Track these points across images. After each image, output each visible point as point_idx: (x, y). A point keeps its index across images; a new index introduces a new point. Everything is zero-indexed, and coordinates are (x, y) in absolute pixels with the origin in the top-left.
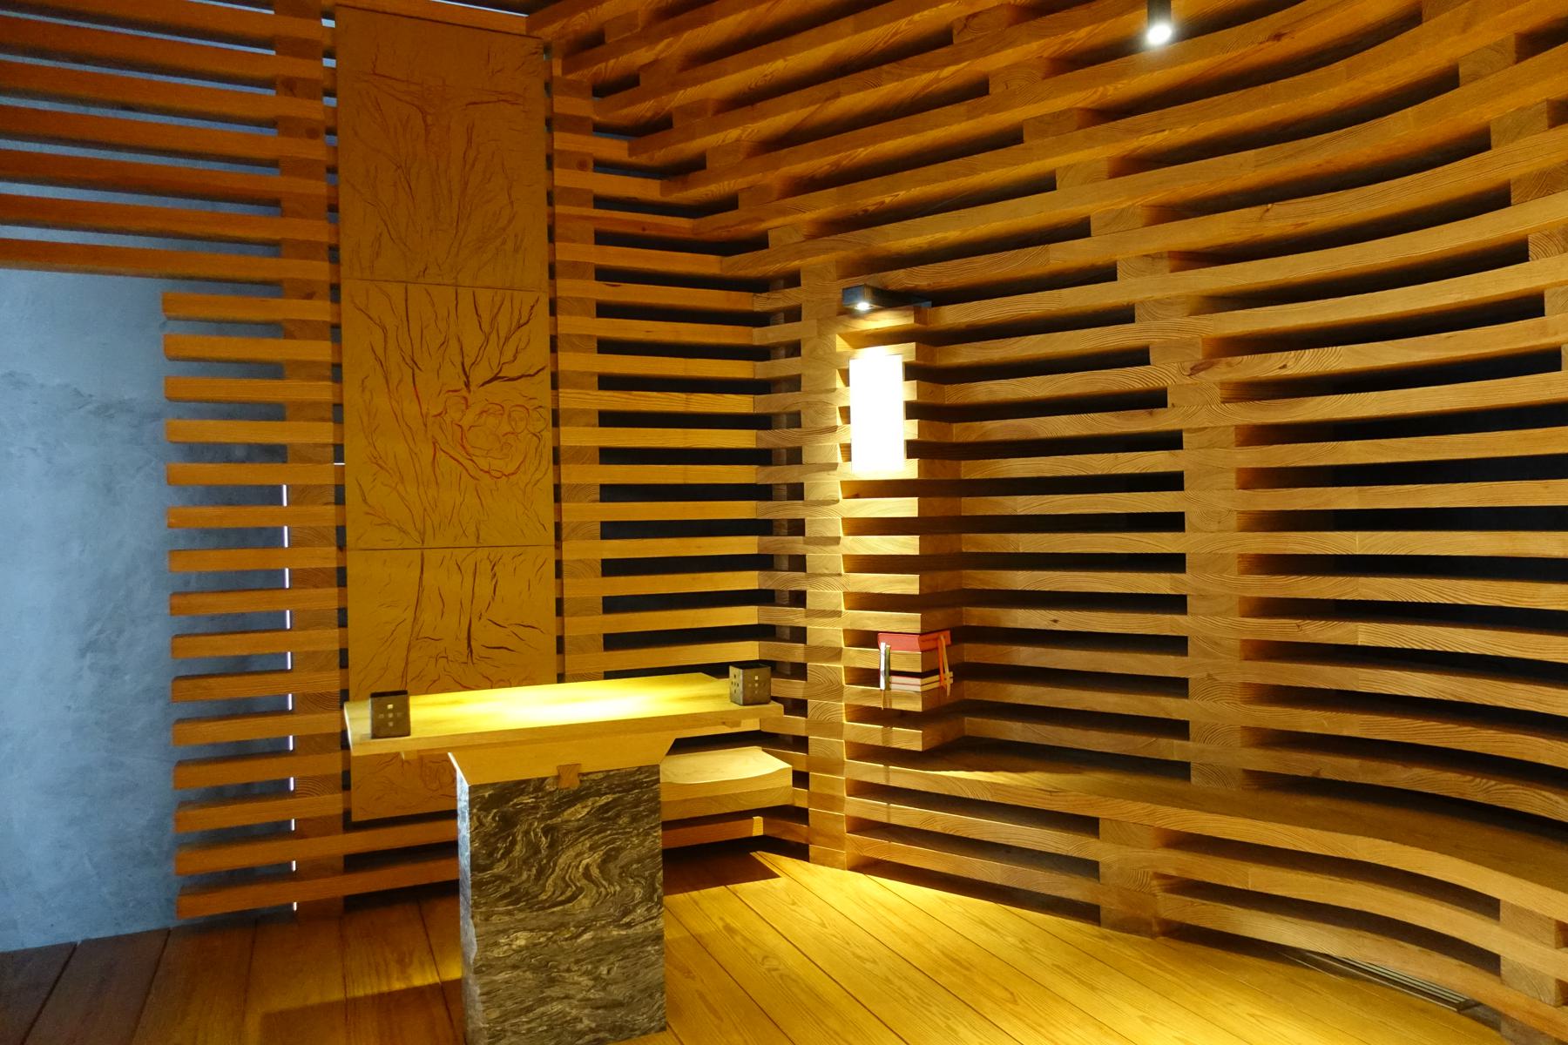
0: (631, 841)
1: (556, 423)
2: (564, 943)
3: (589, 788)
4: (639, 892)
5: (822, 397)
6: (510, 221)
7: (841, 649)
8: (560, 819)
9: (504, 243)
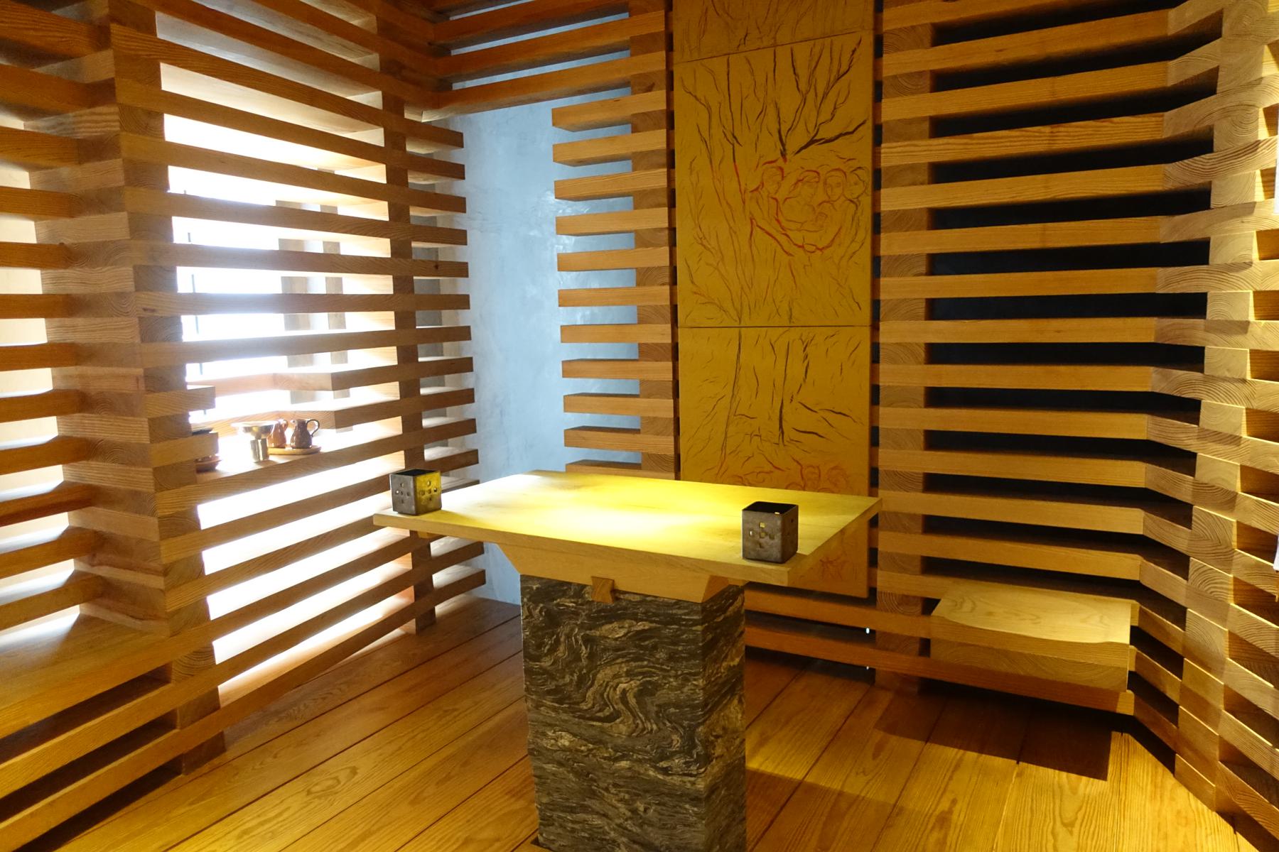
0: (669, 682)
2: (602, 760)
3: (625, 608)
4: (677, 741)
7: (1235, 495)
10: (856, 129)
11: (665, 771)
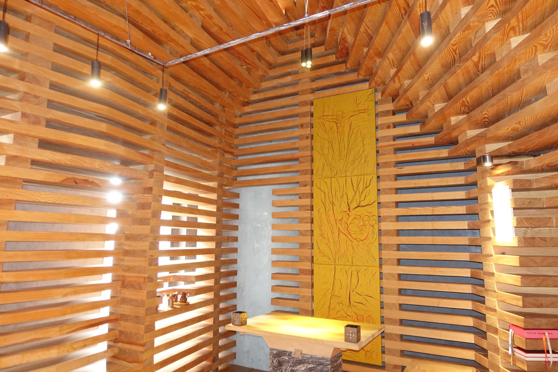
1: (379, 221)
3: (305, 360)
5: (485, 206)
6: (363, 152)
7: (497, 329)
8: (296, 368)
9: (361, 160)
10: (372, 204)
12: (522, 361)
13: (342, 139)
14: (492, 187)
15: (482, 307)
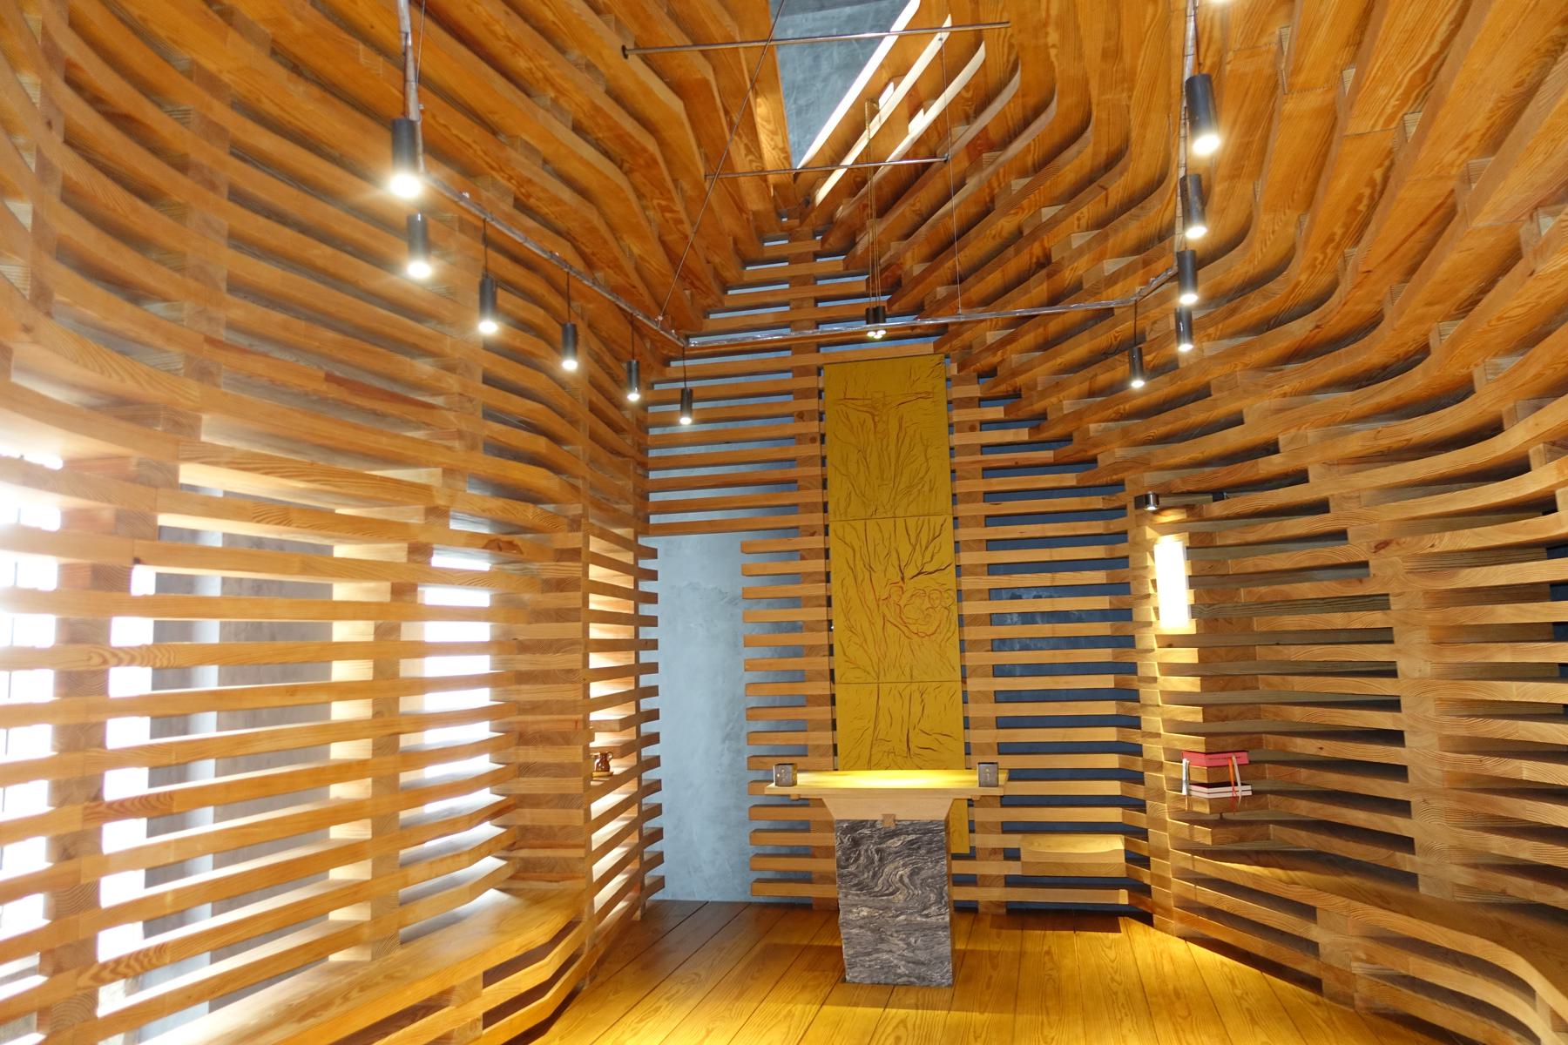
1: (960, 600)
4: (933, 897)
5: (1141, 572)
6: (927, 472)
11: (927, 916)
12: (1201, 802)
13: (885, 447)
14: (1153, 542)
15: (1135, 733)
